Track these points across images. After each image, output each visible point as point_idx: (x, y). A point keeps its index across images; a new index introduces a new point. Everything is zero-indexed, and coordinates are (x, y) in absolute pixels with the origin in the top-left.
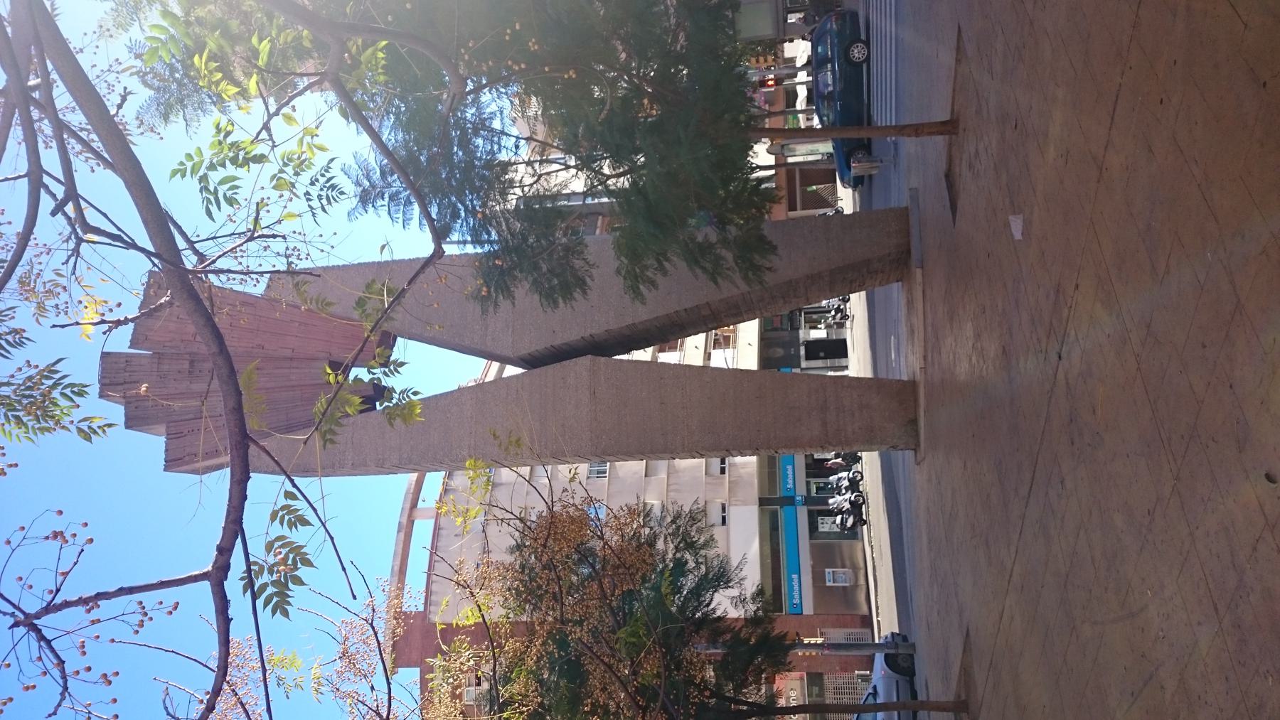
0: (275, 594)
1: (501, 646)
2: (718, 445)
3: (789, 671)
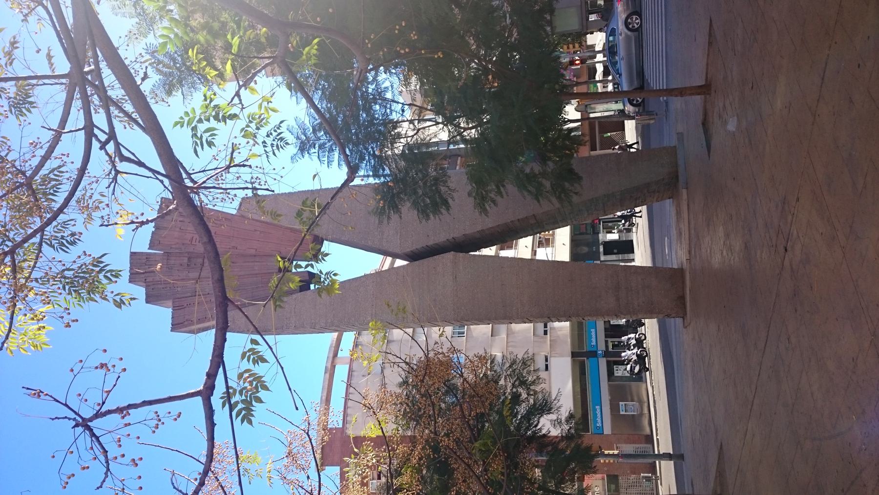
0: (243, 409)
1: (393, 450)
2: (543, 314)
3: (595, 473)
